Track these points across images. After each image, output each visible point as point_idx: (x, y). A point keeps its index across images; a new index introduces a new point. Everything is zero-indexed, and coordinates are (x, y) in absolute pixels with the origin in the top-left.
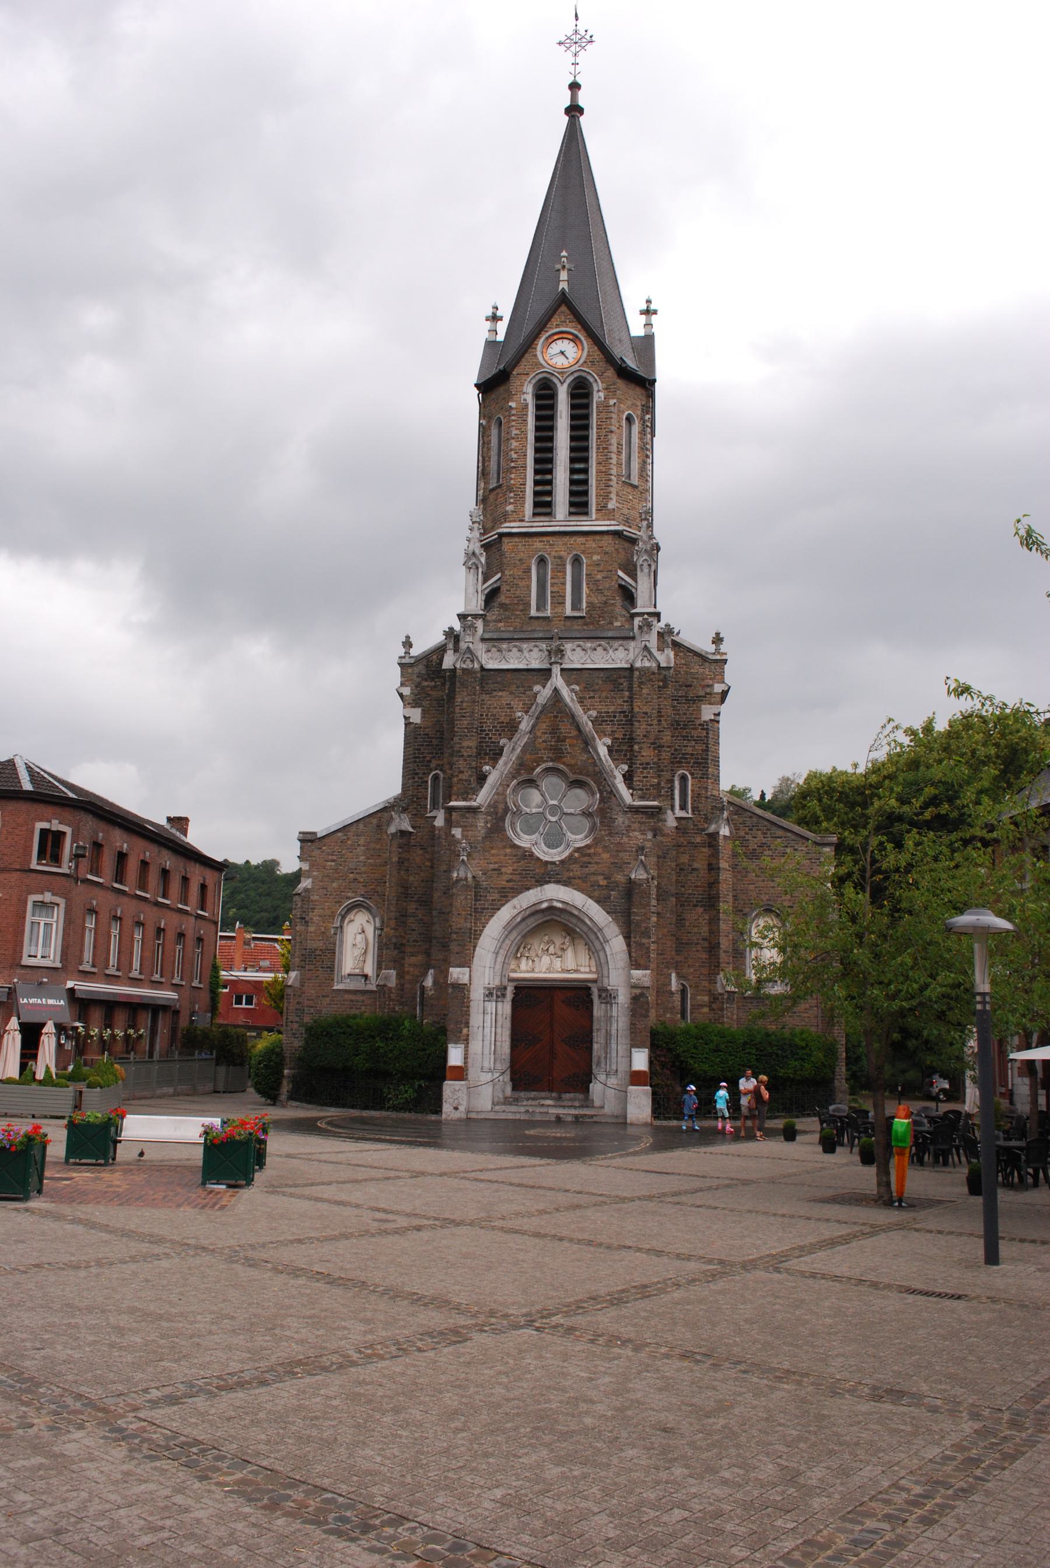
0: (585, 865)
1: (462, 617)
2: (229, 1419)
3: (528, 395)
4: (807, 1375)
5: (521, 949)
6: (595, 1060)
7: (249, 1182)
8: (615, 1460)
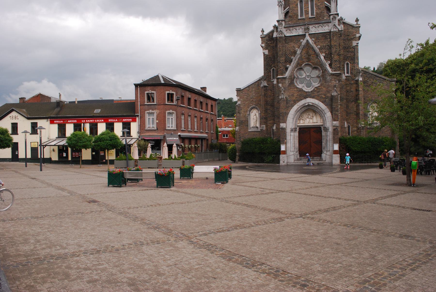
0: (318, 92)
1: (278, 21)
2: (219, 239)
4: (380, 231)
6: (323, 147)
7: (227, 182)
8: (322, 251)
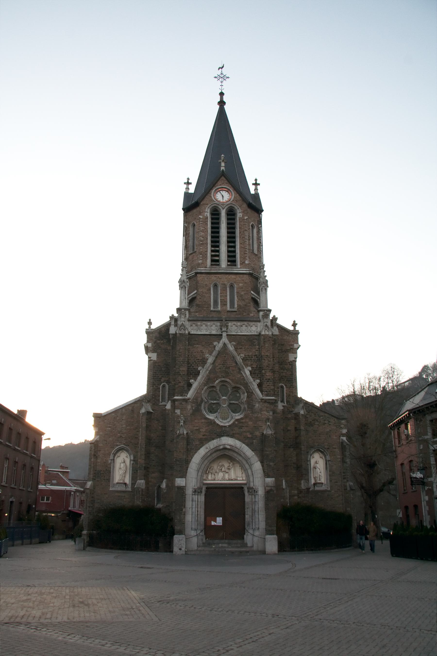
0: (241, 427)
3: (208, 214)
5: (209, 469)
